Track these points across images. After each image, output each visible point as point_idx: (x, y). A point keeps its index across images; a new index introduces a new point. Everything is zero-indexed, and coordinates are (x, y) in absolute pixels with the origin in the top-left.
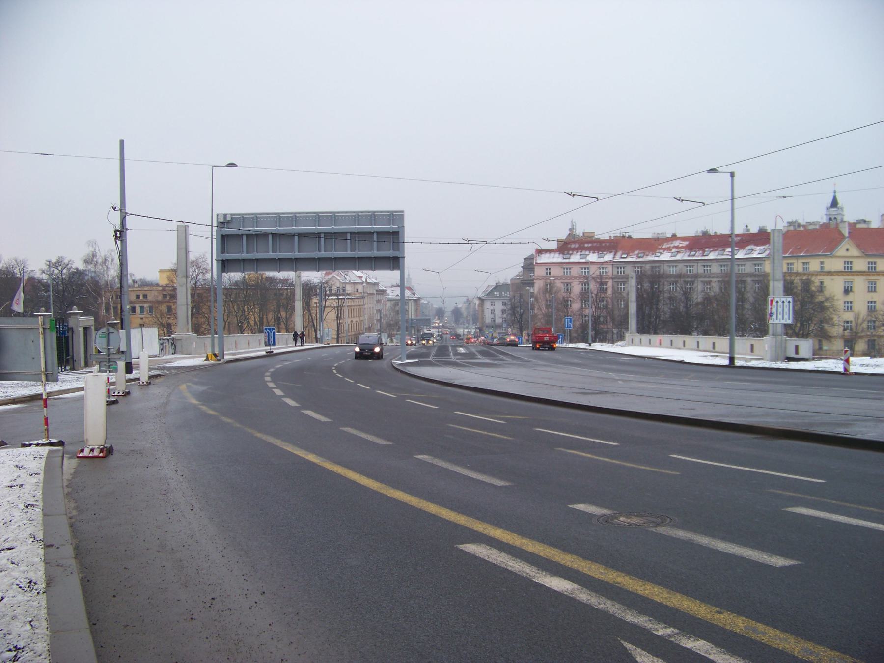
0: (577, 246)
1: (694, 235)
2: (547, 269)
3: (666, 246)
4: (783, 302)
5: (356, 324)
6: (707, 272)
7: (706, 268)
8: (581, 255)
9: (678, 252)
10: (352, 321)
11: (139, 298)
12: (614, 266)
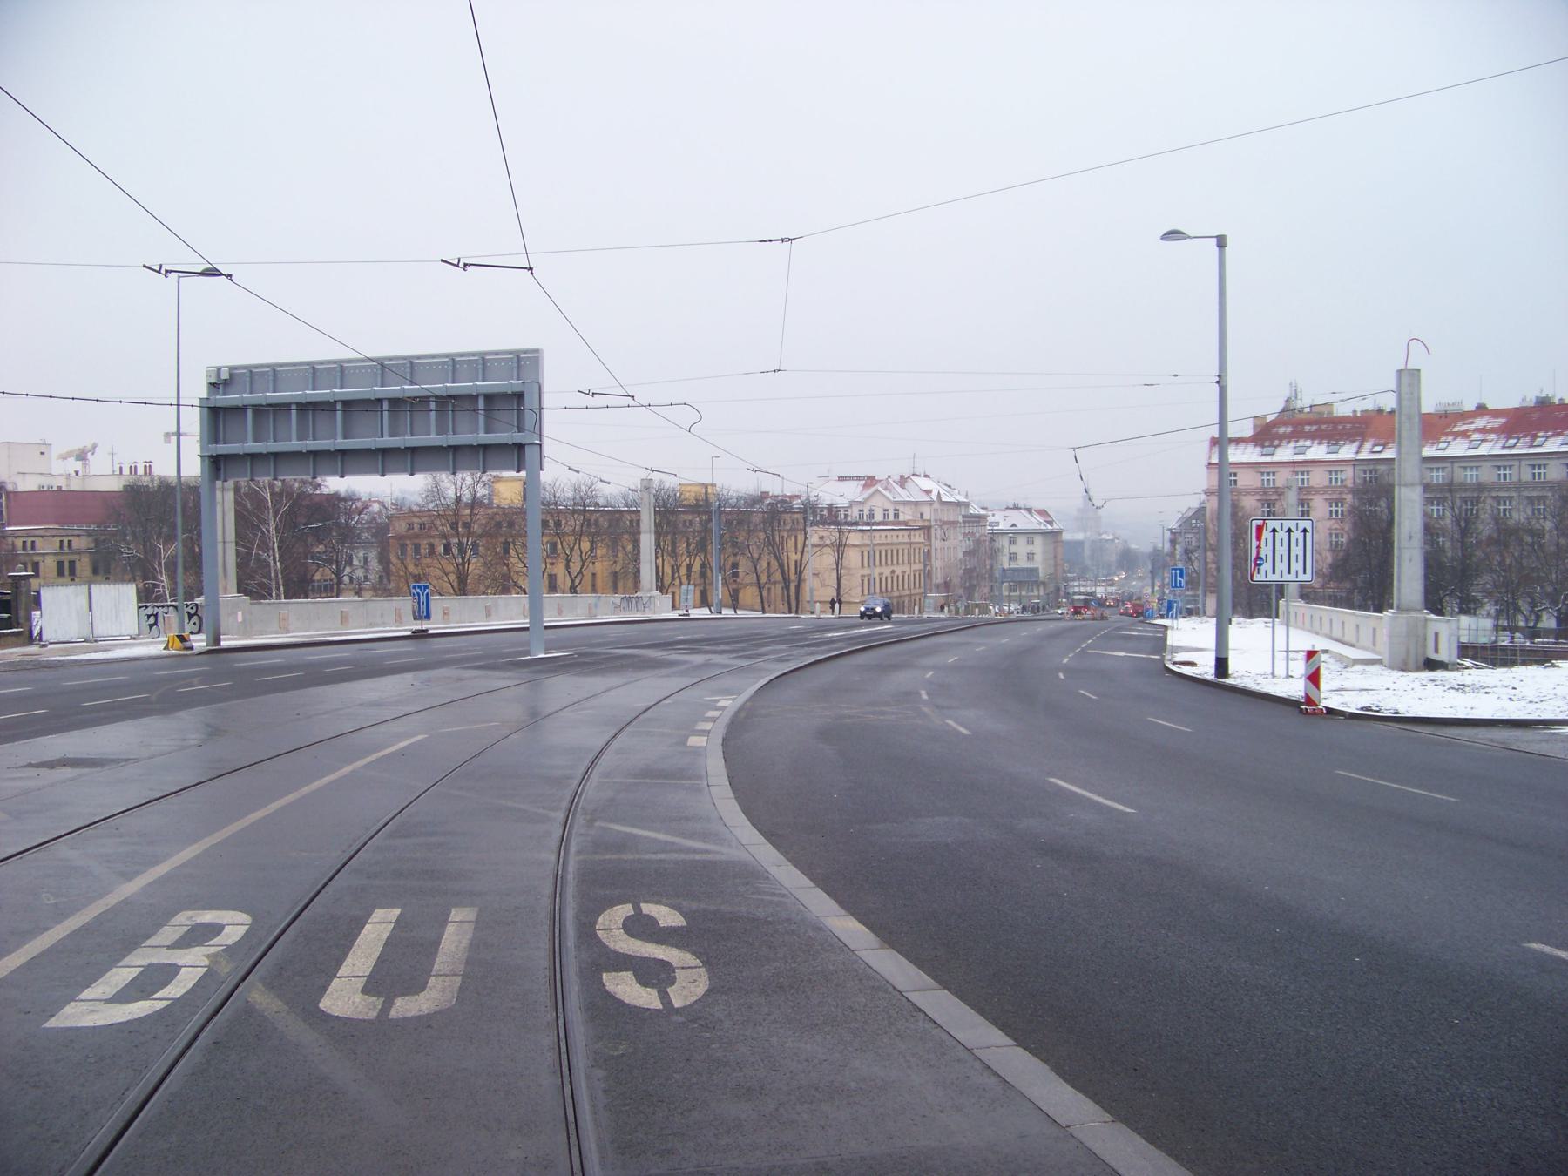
0: (1289, 429)
1: (1517, 405)
3: (1460, 427)
4: (1289, 531)
5: (903, 576)
6: (1539, 478)
7: (1536, 471)
8: (1295, 448)
9: (1483, 441)
10: (893, 572)
12: (1357, 468)
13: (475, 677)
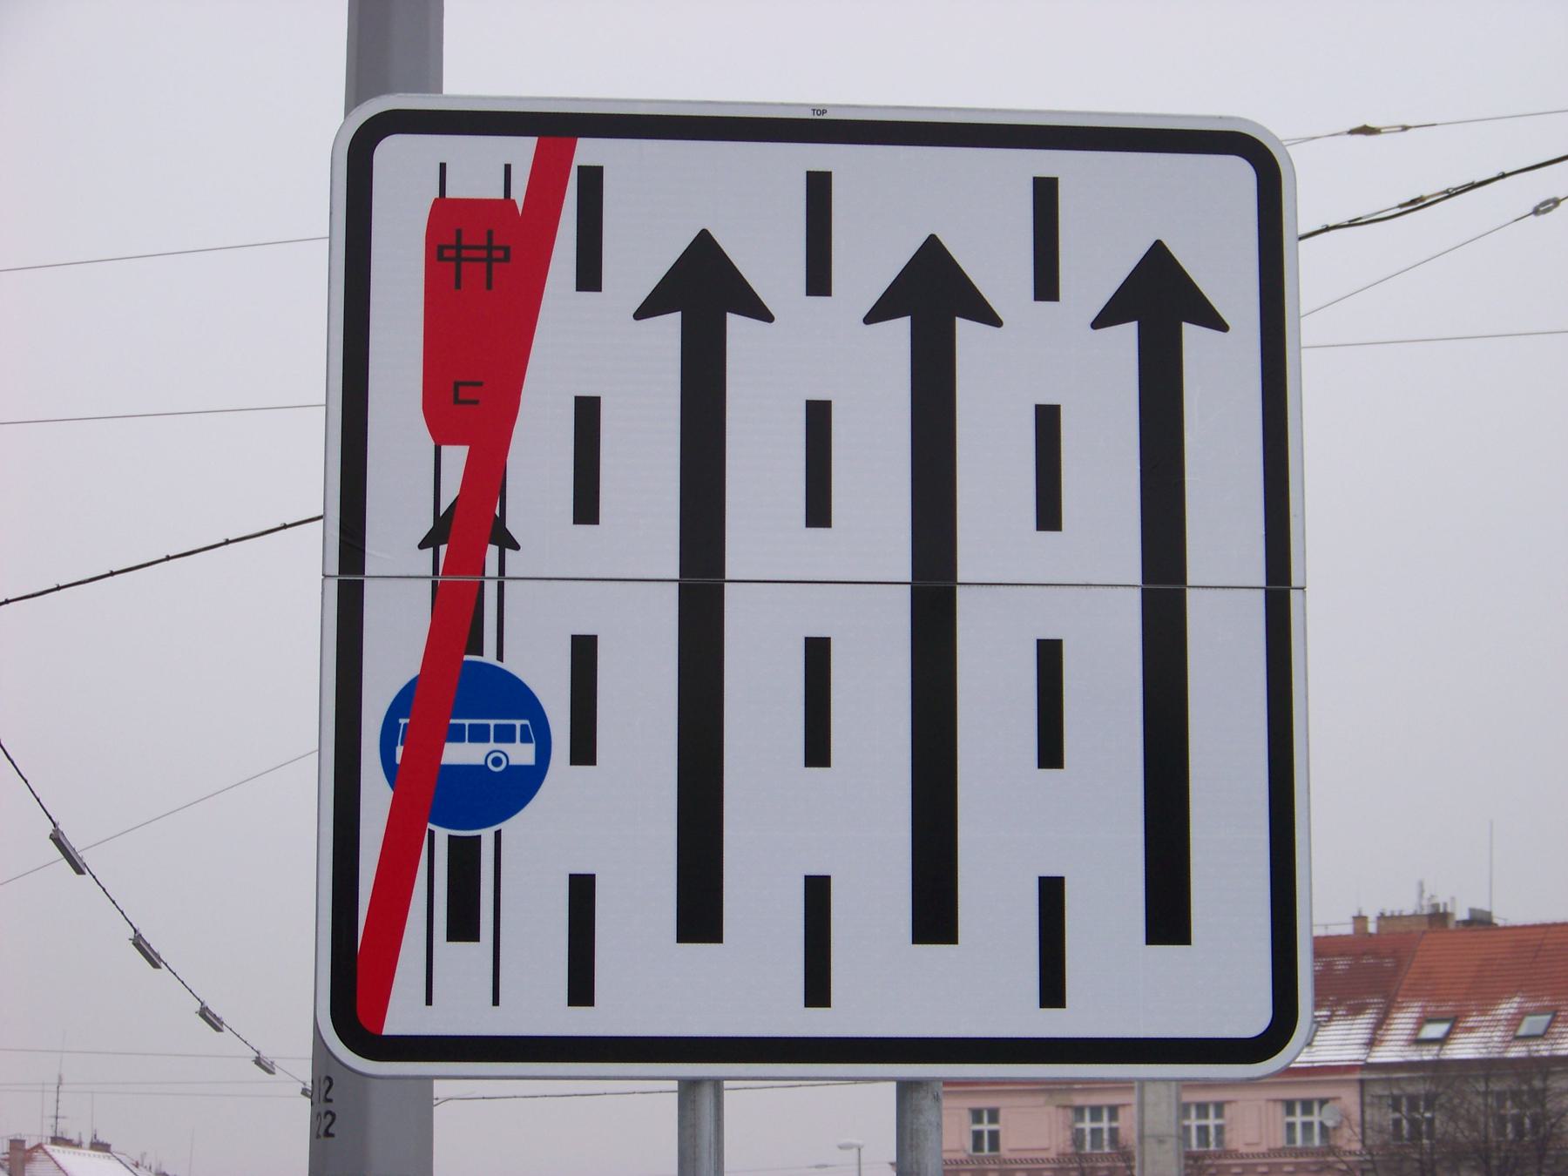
2: (977, 1115)
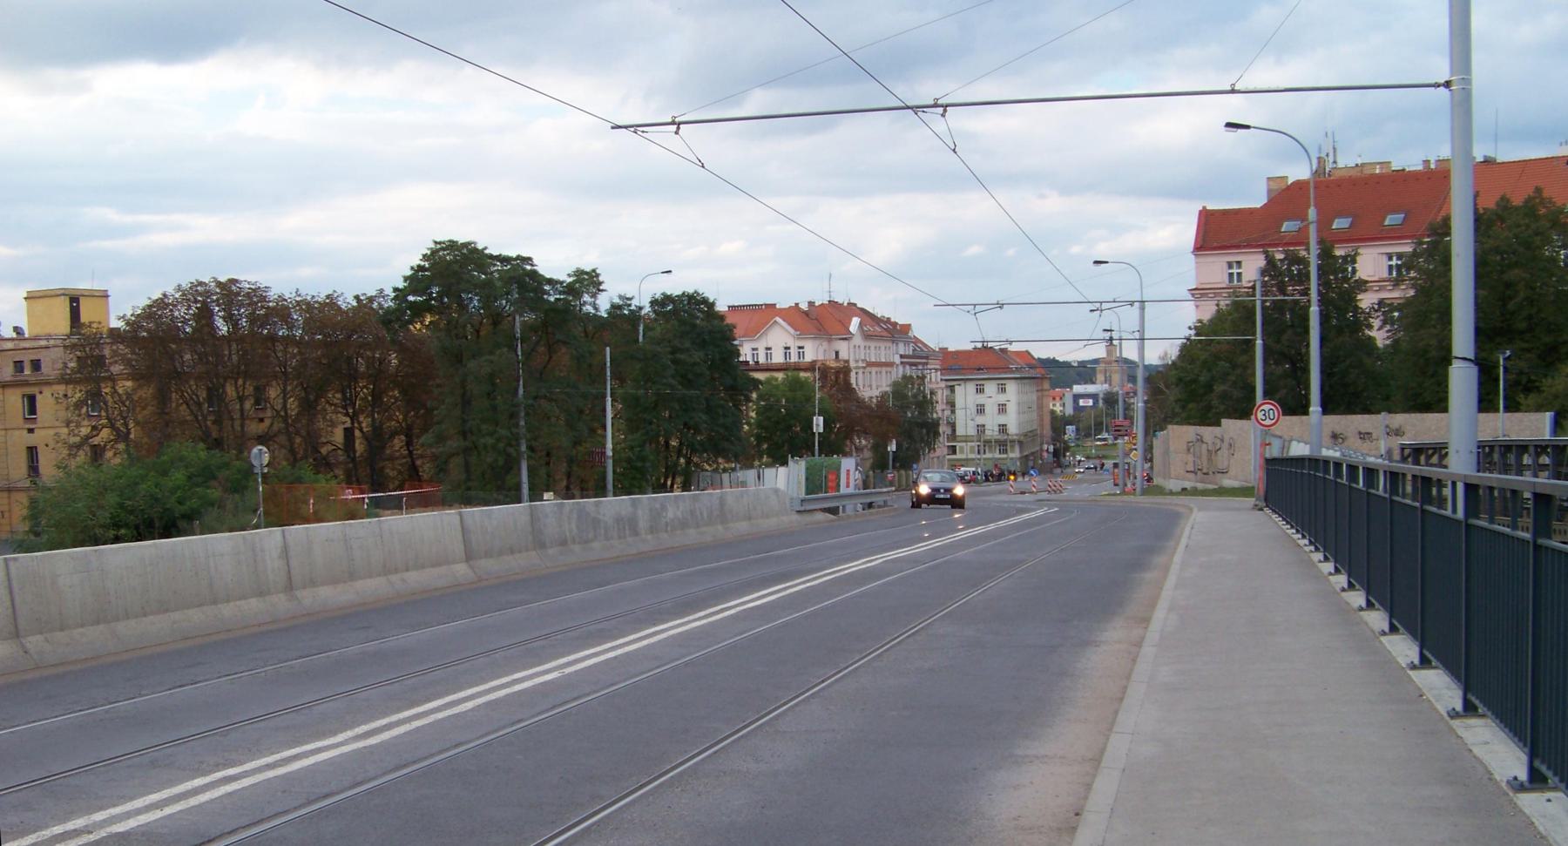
2: (1230, 265)
11: (22, 371)
13: (1311, 164)
